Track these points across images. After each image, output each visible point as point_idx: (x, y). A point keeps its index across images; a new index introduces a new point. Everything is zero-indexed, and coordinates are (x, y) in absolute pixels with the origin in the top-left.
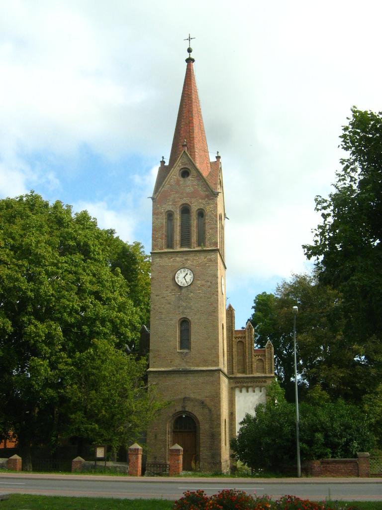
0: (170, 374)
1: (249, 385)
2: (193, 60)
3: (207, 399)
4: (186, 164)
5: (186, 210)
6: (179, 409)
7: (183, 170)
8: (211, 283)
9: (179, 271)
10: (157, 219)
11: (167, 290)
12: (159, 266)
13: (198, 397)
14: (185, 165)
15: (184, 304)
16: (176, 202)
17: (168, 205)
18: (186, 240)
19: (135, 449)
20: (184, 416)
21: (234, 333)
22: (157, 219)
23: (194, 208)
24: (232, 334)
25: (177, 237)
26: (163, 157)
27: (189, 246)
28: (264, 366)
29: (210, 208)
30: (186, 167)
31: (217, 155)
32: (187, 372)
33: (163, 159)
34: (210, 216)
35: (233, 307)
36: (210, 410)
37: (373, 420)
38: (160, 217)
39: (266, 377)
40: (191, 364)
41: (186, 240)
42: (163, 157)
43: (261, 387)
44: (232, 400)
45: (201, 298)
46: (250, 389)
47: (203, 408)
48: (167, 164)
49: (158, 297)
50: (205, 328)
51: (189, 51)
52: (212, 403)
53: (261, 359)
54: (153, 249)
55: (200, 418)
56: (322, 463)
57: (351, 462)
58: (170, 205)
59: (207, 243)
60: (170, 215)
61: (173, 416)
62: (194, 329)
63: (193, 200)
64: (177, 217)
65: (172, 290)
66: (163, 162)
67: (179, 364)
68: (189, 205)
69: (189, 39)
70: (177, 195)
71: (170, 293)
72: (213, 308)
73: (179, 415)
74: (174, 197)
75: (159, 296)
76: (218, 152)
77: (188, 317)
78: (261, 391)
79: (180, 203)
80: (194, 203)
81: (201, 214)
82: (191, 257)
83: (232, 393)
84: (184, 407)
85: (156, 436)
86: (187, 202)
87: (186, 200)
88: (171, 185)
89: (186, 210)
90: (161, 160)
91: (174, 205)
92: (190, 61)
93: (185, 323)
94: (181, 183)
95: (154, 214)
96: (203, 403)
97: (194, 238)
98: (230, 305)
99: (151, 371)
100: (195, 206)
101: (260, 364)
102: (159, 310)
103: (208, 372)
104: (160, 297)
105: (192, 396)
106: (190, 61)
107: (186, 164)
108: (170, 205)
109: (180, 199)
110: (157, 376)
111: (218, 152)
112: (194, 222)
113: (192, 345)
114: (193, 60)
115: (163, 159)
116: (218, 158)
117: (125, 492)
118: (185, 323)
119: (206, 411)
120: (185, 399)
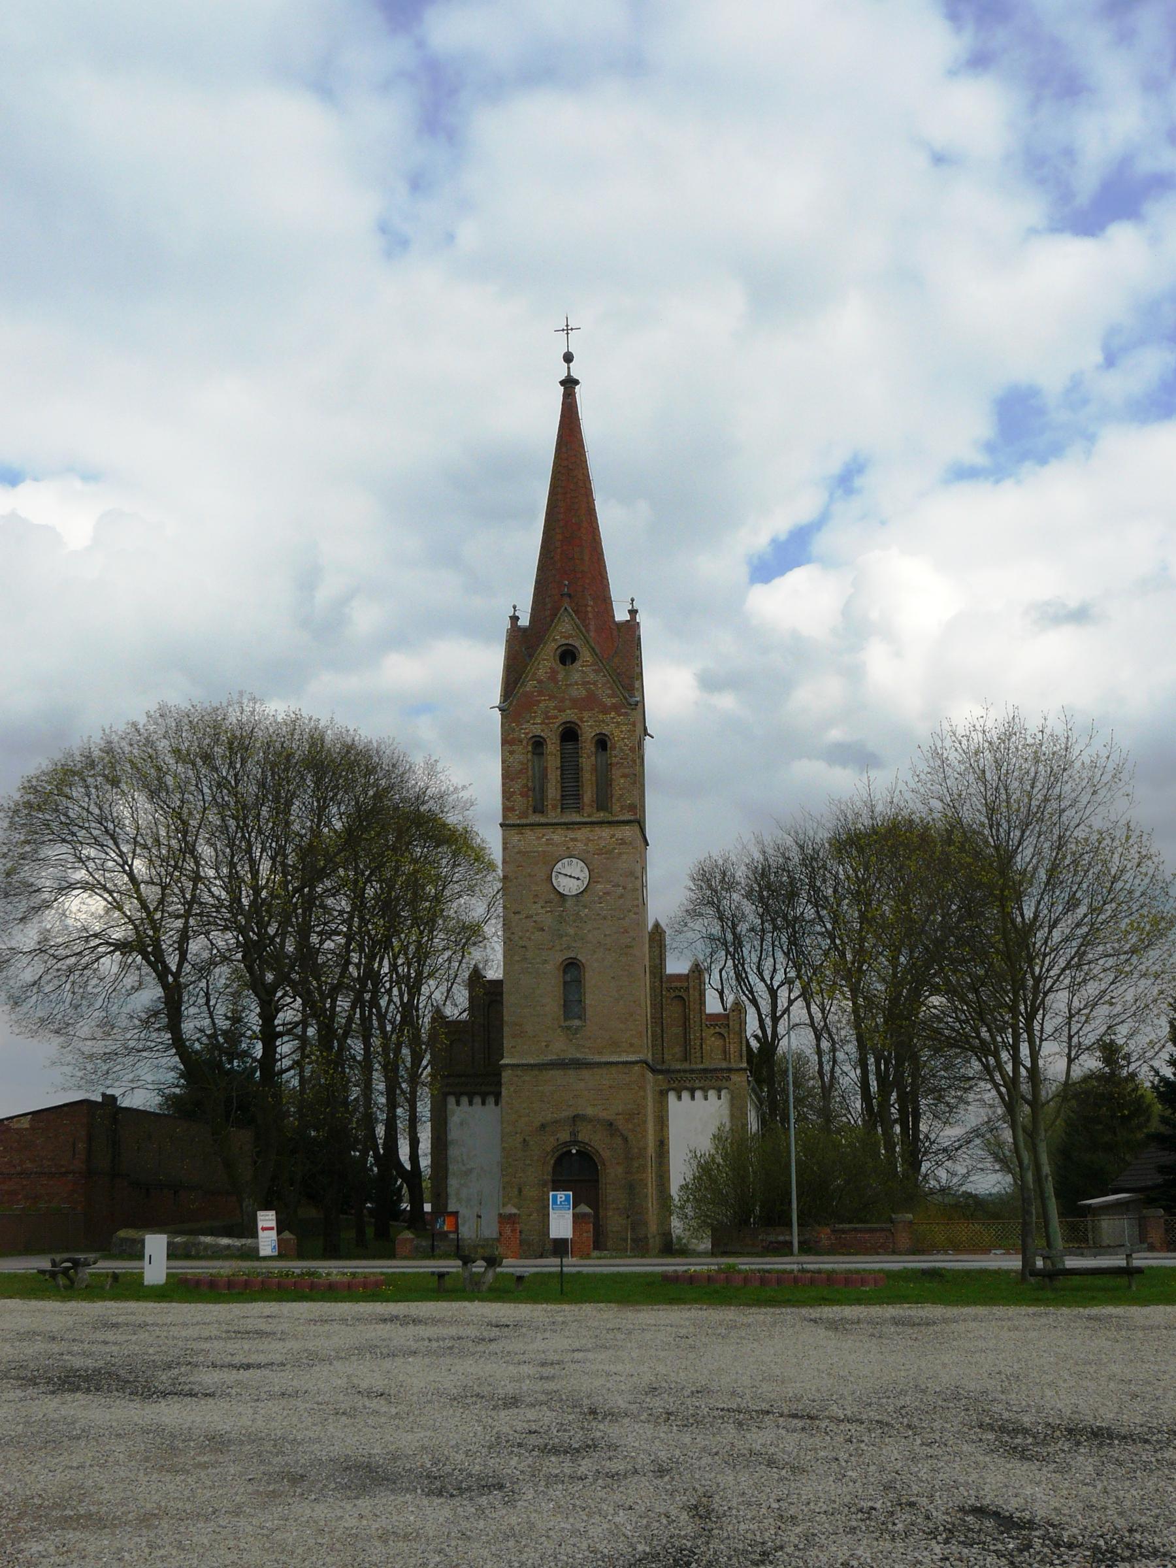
0: (546, 1069)
1: (697, 1084)
2: (577, 382)
3: (618, 1117)
4: (571, 636)
5: (570, 734)
6: (565, 1136)
7: (564, 648)
8: (624, 888)
9: (560, 863)
10: (512, 753)
11: (535, 903)
12: (518, 853)
13: (604, 1115)
14: (567, 638)
15: (571, 931)
16: (548, 718)
17: (534, 724)
18: (571, 796)
19: (510, 1214)
20: (574, 1151)
21: (664, 979)
22: (512, 753)
23: (588, 732)
24: (662, 982)
25: (553, 791)
26: (515, 607)
27: (579, 810)
28: (725, 1046)
29: (622, 732)
30: (570, 641)
31: (630, 608)
32: (578, 1064)
33: (515, 610)
34: (622, 750)
35: (659, 921)
36: (625, 1140)
37: (1148, 928)
38: (519, 749)
39: (730, 1070)
40: (587, 1050)
41: (571, 796)
42: (515, 607)
43: (719, 1091)
44: (662, 1117)
45: (605, 918)
46: (698, 1094)
47: (612, 1135)
48: (524, 622)
49: (517, 917)
50: (613, 978)
51: (568, 358)
52: (630, 1126)
53: (720, 1034)
54: (504, 817)
55: (606, 1154)
56: (834, 1231)
57: (882, 1230)
58: (537, 724)
59: (616, 808)
60: (538, 744)
61: (552, 1151)
62: (591, 979)
63: (586, 715)
64: (553, 746)
65: (546, 902)
66: (514, 619)
67: (561, 1047)
68: (577, 724)
69: (567, 330)
70: (552, 704)
71: (542, 907)
72: (629, 940)
73: (565, 1150)
74: (547, 707)
75: (518, 913)
76: (633, 600)
77: (579, 957)
78: (719, 1098)
79: (559, 721)
80: (587, 721)
81: (602, 743)
82: (582, 834)
83: (661, 1103)
84: (573, 1134)
85: (520, 1191)
86: (574, 718)
87: (570, 715)
88: (540, 682)
89: (570, 734)
90: (512, 614)
91: (547, 724)
92: (569, 384)
93: (572, 967)
94: (560, 677)
95: (505, 742)
96: (611, 1124)
97: (588, 795)
98: (657, 921)
99: (507, 1065)
100: (591, 727)
101: (719, 1042)
102: (521, 943)
103: (620, 1066)
104: (521, 916)
105: (590, 1111)
106: (569, 384)
107: (571, 636)
108: (537, 724)
109: (560, 711)
110: (519, 1073)
111: (633, 600)
112: (588, 760)
113: (589, 1012)
114: (577, 382)
115: (515, 610)
116: (633, 612)
117: (106, 1343)
118: (572, 967)
119: (619, 1140)
120: (576, 1118)
